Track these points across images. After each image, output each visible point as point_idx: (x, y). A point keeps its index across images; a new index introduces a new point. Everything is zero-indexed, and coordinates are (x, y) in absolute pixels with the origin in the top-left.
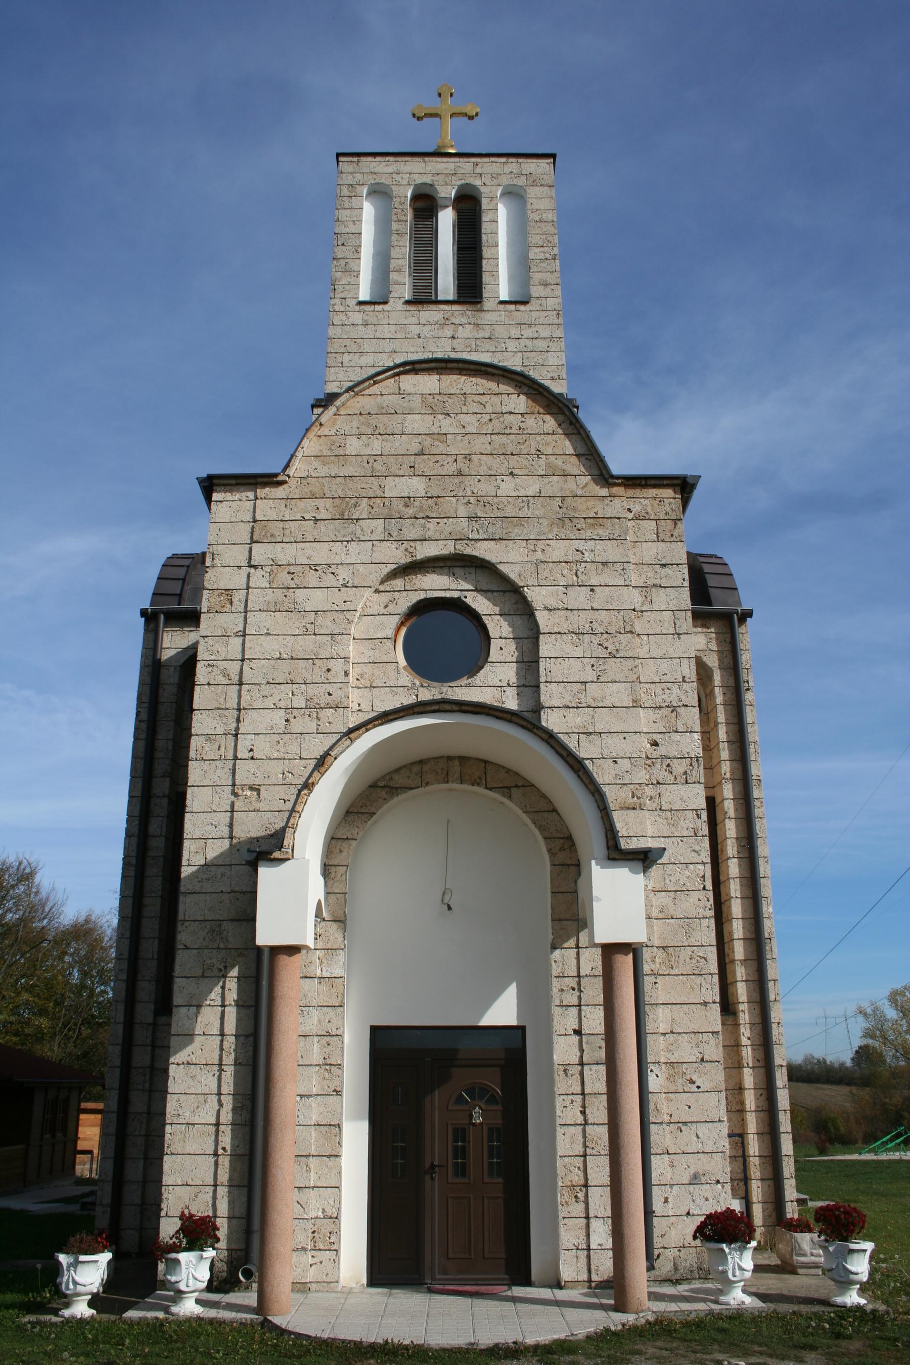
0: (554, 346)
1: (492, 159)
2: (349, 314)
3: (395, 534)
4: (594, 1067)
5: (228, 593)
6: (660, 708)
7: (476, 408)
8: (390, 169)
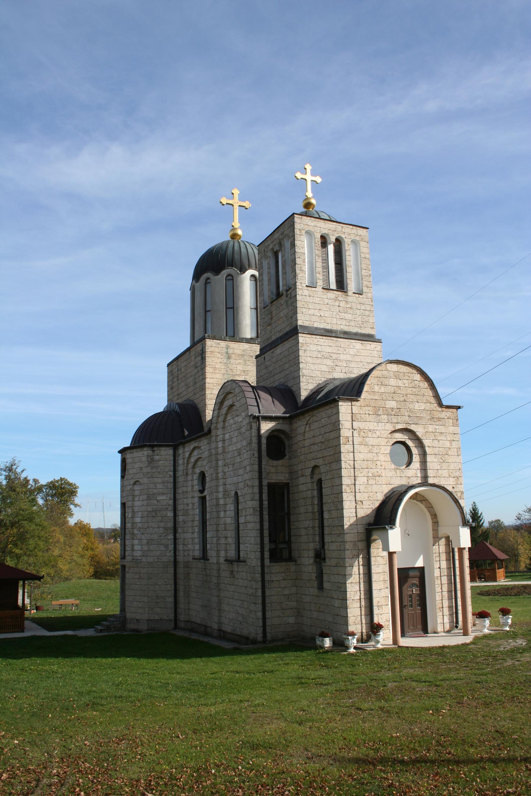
8: (313, 224)
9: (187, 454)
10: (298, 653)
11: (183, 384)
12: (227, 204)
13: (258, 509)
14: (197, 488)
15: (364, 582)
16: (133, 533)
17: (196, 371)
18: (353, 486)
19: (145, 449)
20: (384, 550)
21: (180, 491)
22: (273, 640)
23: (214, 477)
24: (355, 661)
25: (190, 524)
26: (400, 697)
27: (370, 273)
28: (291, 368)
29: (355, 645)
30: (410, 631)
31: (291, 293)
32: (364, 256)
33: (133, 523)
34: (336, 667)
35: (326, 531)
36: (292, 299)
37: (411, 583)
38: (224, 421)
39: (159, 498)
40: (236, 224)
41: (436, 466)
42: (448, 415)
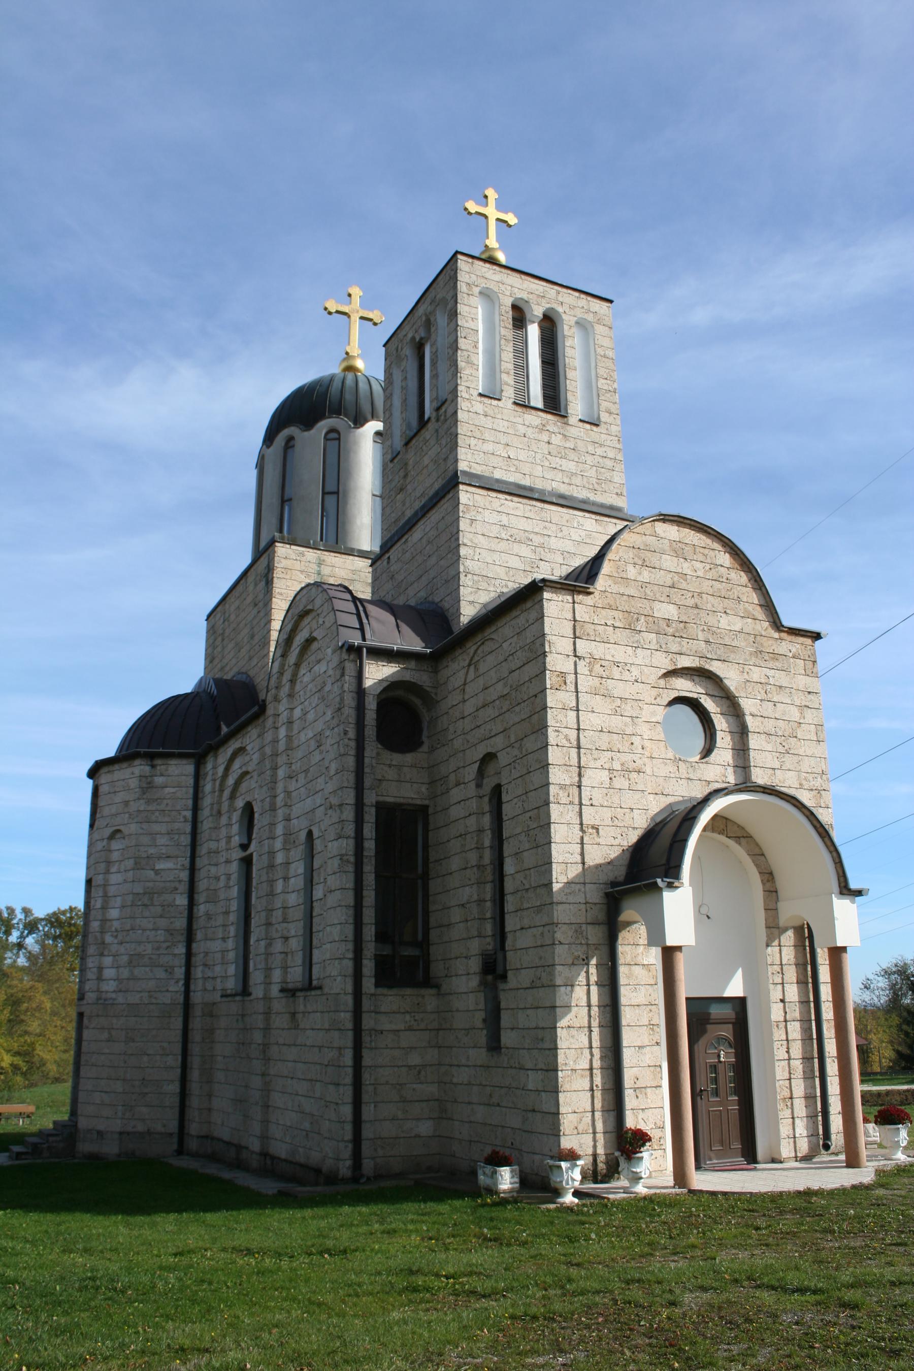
0: (618, 467)
1: (570, 291)
2: (474, 403)
3: (664, 646)
4: (793, 1023)
5: (563, 674)
6: (812, 790)
7: (702, 558)
9: (221, 770)
10: (431, 1206)
11: (231, 646)
12: (338, 312)
13: (352, 859)
14: (236, 840)
15: (600, 1026)
16: (103, 943)
17: (255, 611)
18: (576, 790)
19: (137, 762)
20: (651, 943)
21: (203, 850)
22: (378, 1177)
23: (267, 807)
24: (578, 1228)
25: (220, 920)
26: (735, 1349)
27: (615, 385)
28: (442, 563)
29: (577, 1184)
30: (712, 1155)
31: (445, 412)
32: (602, 353)
33: (104, 921)
34: (524, 1244)
35: (510, 903)
36: (448, 422)
37: (717, 1036)
38: (293, 681)
39: (160, 866)
40: (354, 350)
41: (770, 760)
42: (794, 650)
